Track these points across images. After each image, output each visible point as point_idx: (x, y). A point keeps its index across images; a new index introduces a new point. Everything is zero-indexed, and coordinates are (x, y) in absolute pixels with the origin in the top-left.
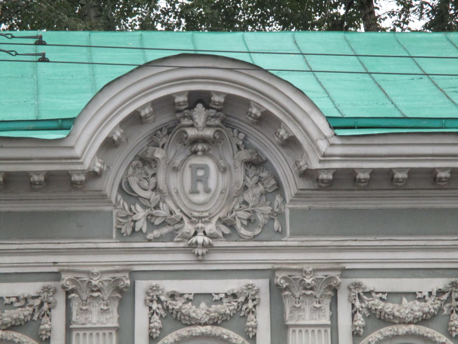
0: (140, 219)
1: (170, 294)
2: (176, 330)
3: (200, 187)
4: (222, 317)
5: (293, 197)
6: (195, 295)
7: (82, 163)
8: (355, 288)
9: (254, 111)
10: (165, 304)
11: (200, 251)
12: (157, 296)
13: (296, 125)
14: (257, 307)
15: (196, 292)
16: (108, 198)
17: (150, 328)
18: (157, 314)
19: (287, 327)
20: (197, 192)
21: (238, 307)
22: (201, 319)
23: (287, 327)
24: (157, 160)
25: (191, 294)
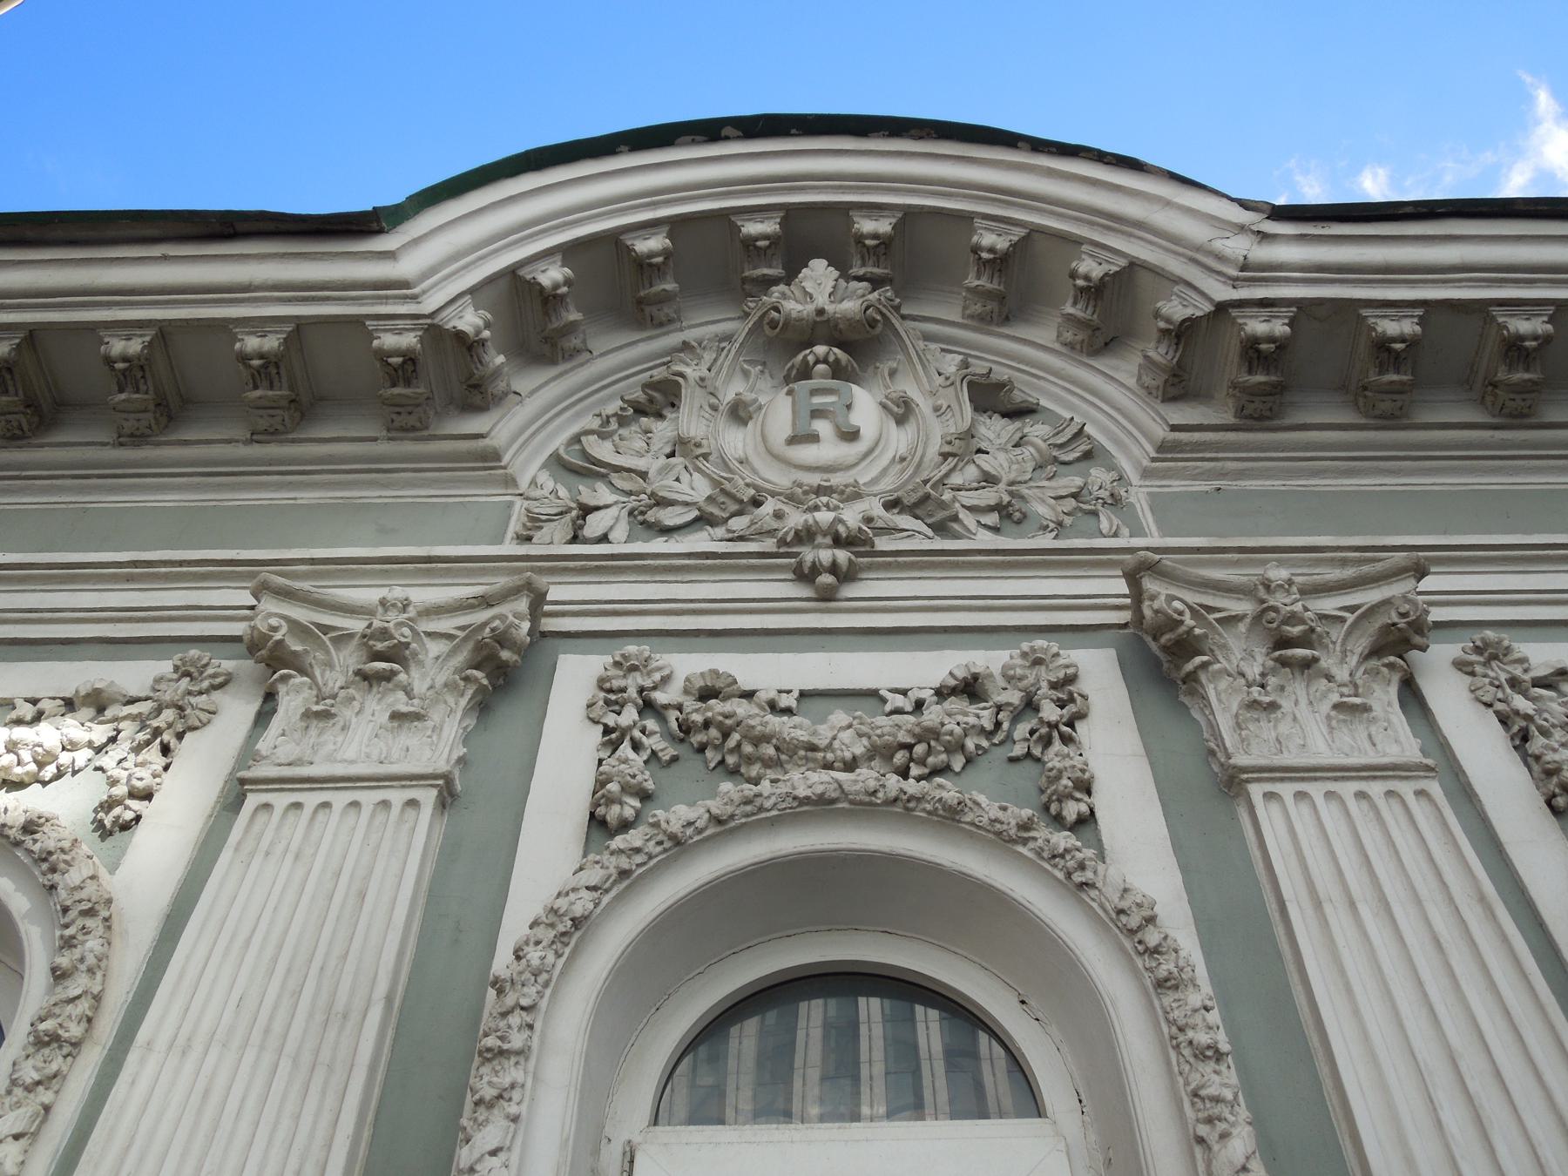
0: (607, 507)
1: (699, 683)
2: (695, 135)
3: (823, 427)
4: (930, 751)
5: (1154, 460)
6: (804, 694)
7: (414, 298)
8: (1486, 664)
9: (988, 239)
10: (673, 715)
11: (826, 579)
12: (641, 690)
13: (1131, 235)
14: (1079, 725)
15: (809, 685)
16: (504, 468)
17: (601, 783)
18: (636, 746)
19: (1233, 783)
20: (814, 438)
21: (998, 725)
22: (830, 744)
23: (1233, 783)
24: (681, 380)
25: (789, 692)
